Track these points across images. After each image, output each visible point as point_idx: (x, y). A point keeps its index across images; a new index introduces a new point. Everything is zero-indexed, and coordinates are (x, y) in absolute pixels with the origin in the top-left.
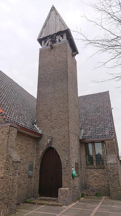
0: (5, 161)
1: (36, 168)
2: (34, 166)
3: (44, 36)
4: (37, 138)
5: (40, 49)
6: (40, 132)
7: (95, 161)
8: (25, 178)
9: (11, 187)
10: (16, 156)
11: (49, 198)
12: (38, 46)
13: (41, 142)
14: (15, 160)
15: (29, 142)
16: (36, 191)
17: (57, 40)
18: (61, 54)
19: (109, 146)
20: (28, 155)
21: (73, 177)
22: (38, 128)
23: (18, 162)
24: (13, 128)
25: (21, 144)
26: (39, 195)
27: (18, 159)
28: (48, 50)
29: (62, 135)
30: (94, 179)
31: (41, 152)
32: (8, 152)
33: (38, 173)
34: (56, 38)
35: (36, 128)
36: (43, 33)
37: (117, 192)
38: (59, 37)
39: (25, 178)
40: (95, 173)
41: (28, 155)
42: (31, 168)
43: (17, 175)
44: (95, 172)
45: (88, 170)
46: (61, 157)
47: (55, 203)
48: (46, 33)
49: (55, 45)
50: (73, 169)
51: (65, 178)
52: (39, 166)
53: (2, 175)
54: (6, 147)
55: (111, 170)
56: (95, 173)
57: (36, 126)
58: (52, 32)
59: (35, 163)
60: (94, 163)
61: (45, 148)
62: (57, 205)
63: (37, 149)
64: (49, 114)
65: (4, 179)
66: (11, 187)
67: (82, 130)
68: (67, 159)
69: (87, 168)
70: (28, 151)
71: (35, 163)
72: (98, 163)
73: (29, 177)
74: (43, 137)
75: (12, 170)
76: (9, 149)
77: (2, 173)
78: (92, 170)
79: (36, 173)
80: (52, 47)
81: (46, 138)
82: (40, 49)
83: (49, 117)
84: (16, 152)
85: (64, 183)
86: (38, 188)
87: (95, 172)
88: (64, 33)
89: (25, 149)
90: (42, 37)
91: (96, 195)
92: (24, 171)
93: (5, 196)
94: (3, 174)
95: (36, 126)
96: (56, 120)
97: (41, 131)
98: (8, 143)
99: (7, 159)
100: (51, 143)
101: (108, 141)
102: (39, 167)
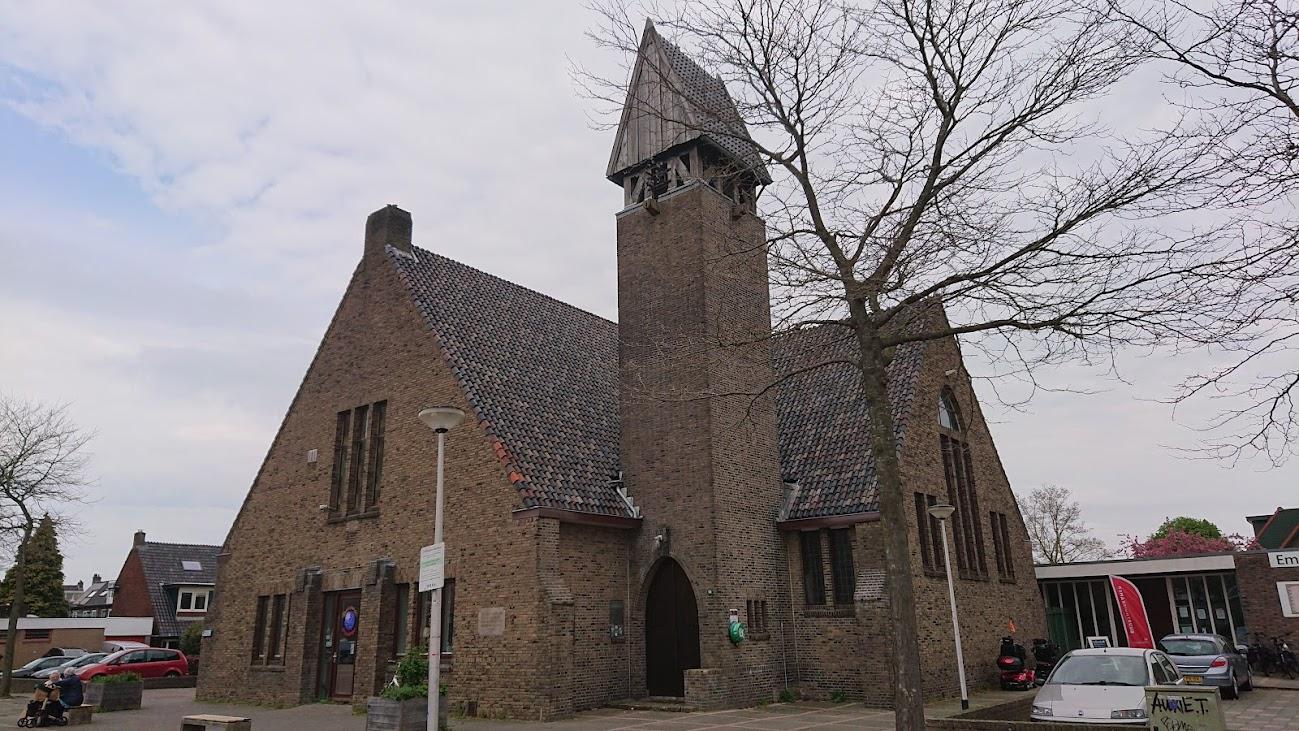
0: (537, 603)
1: (633, 619)
2: (628, 612)
3: (627, 160)
4: (631, 529)
5: (617, 215)
6: (635, 512)
7: (830, 593)
8: (602, 645)
9: (554, 660)
10: (559, 591)
11: (674, 698)
12: (616, 198)
13: (641, 541)
14: (78, 665)
15: (602, 546)
16: (638, 680)
17: (671, 175)
18: (684, 238)
19: (868, 543)
20: (603, 581)
21: (735, 641)
22: (629, 501)
23: (565, 604)
24: (546, 521)
25: (580, 555)
26: (648, 691)
27: (567, 598)
28: (644, 217)
29: (696, 521)
30: (828, 648)
31: (643, 572)
32: (540, 581)
33: (641, 631)
34: (669, 167)
35: (622, 500)
36: (624, 151)
37: (881, 685)
38: (677, 166)
39: (602, 645)
40: (831, 632)
41: (603, 581)
42: (617, 617)
43: (569, 633)
44: (829, 628)
45: (808, 620)
46: (694, 586)
47: (678, 706)
48: (633, 150)
49: (665, 199)
50: (733, 618)
51: (706, 642)
52: (643, 613)
53: (534, 635)
54: (535, 570)
55: (864, 621)
56: (831, 632)
57: (622, 492)
58: (651, 150)
59: (628, 603)
60: (828, 599)
61: (652, 561)
62: (680, 711)
63: (634, 563)
64: (658, 454)
65: (539, 644)
66: (554, 660)
67: (797, 487)
68: (710, 592)
69: (807, 615)
70: (603, 570)
71: (628, 603)
72: (838, 600)
73: (614, 641)
74: (644, 528)
75: (554, 622)
76: (543, 574)
77: (532, 630)
78: (823, 622)
79: (632, 631)
80: (652, 211)
81: (653, 529)
82: (617, 215)
83: (657, 464)
84: (561, 581)
85: (706, 657)
86: (643, 673)
87: (829, 628)
88: (692, 149)
89: (591, 566)
90: (620, 168)
91: (835, 696)
92: (595, 627)
93: (545, 680)
94: (535, 632)
95: (622, 492)
96: (677, 474)
97: (638, 508)
98: (538, 559)
99: (541, 599)
100: (665, 545)
101: (864, 526)
102: (641, 616)
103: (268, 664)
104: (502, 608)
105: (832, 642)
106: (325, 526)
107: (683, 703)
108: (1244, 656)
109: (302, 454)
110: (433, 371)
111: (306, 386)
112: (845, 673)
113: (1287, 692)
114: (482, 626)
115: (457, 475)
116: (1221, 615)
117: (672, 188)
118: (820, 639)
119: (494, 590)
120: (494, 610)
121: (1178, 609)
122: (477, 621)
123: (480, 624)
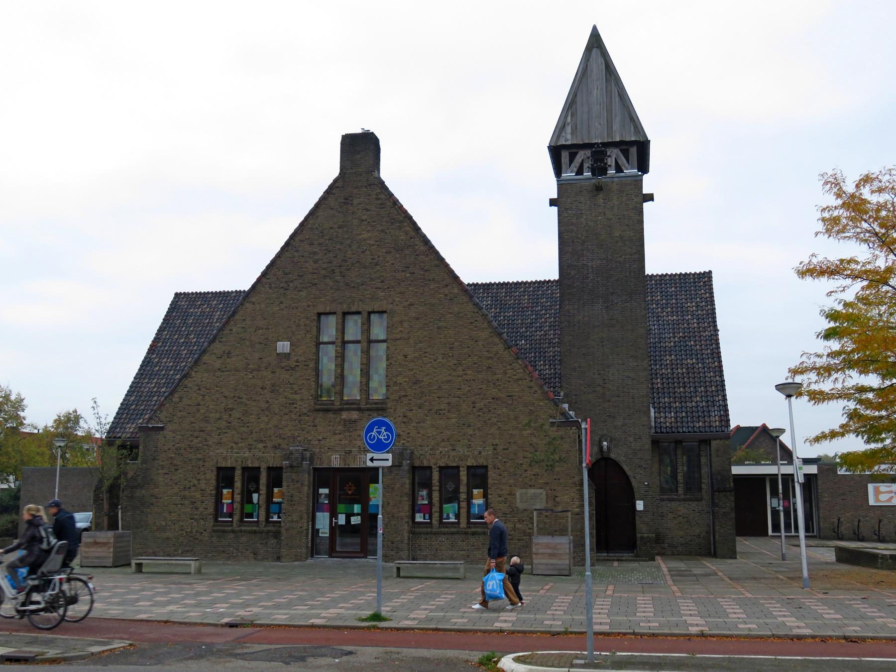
3: (568, 139)
17: (611, 161)
45: (664, 503)
56: (680, 511)
60: (679, 489)
68: (646, 483)
69: (662, 500)
72: (688, 489)
101: (718, 442)
103: (265, 527)
104: (542, 490)
105: (681, 518)
106: (310, 411)
107: (597, 556)
108: (411, 536)
109: (269, 344)
110: (446, 295)
111: (264, 280)
112: (689, 538)
113: (411, 580)
114: (521, 502)
115: (484, 387)
116: (775, 502)
117: (611, 172)
118: (671, 516)
119: (533, 477)
120: (532, 491)
121: (771, 498)
122: (515, 498)
123: (518, 501)
